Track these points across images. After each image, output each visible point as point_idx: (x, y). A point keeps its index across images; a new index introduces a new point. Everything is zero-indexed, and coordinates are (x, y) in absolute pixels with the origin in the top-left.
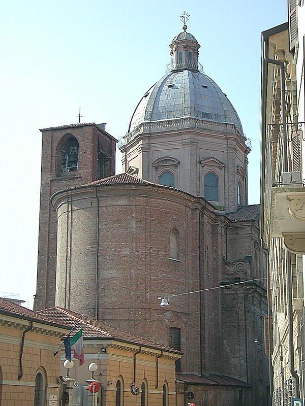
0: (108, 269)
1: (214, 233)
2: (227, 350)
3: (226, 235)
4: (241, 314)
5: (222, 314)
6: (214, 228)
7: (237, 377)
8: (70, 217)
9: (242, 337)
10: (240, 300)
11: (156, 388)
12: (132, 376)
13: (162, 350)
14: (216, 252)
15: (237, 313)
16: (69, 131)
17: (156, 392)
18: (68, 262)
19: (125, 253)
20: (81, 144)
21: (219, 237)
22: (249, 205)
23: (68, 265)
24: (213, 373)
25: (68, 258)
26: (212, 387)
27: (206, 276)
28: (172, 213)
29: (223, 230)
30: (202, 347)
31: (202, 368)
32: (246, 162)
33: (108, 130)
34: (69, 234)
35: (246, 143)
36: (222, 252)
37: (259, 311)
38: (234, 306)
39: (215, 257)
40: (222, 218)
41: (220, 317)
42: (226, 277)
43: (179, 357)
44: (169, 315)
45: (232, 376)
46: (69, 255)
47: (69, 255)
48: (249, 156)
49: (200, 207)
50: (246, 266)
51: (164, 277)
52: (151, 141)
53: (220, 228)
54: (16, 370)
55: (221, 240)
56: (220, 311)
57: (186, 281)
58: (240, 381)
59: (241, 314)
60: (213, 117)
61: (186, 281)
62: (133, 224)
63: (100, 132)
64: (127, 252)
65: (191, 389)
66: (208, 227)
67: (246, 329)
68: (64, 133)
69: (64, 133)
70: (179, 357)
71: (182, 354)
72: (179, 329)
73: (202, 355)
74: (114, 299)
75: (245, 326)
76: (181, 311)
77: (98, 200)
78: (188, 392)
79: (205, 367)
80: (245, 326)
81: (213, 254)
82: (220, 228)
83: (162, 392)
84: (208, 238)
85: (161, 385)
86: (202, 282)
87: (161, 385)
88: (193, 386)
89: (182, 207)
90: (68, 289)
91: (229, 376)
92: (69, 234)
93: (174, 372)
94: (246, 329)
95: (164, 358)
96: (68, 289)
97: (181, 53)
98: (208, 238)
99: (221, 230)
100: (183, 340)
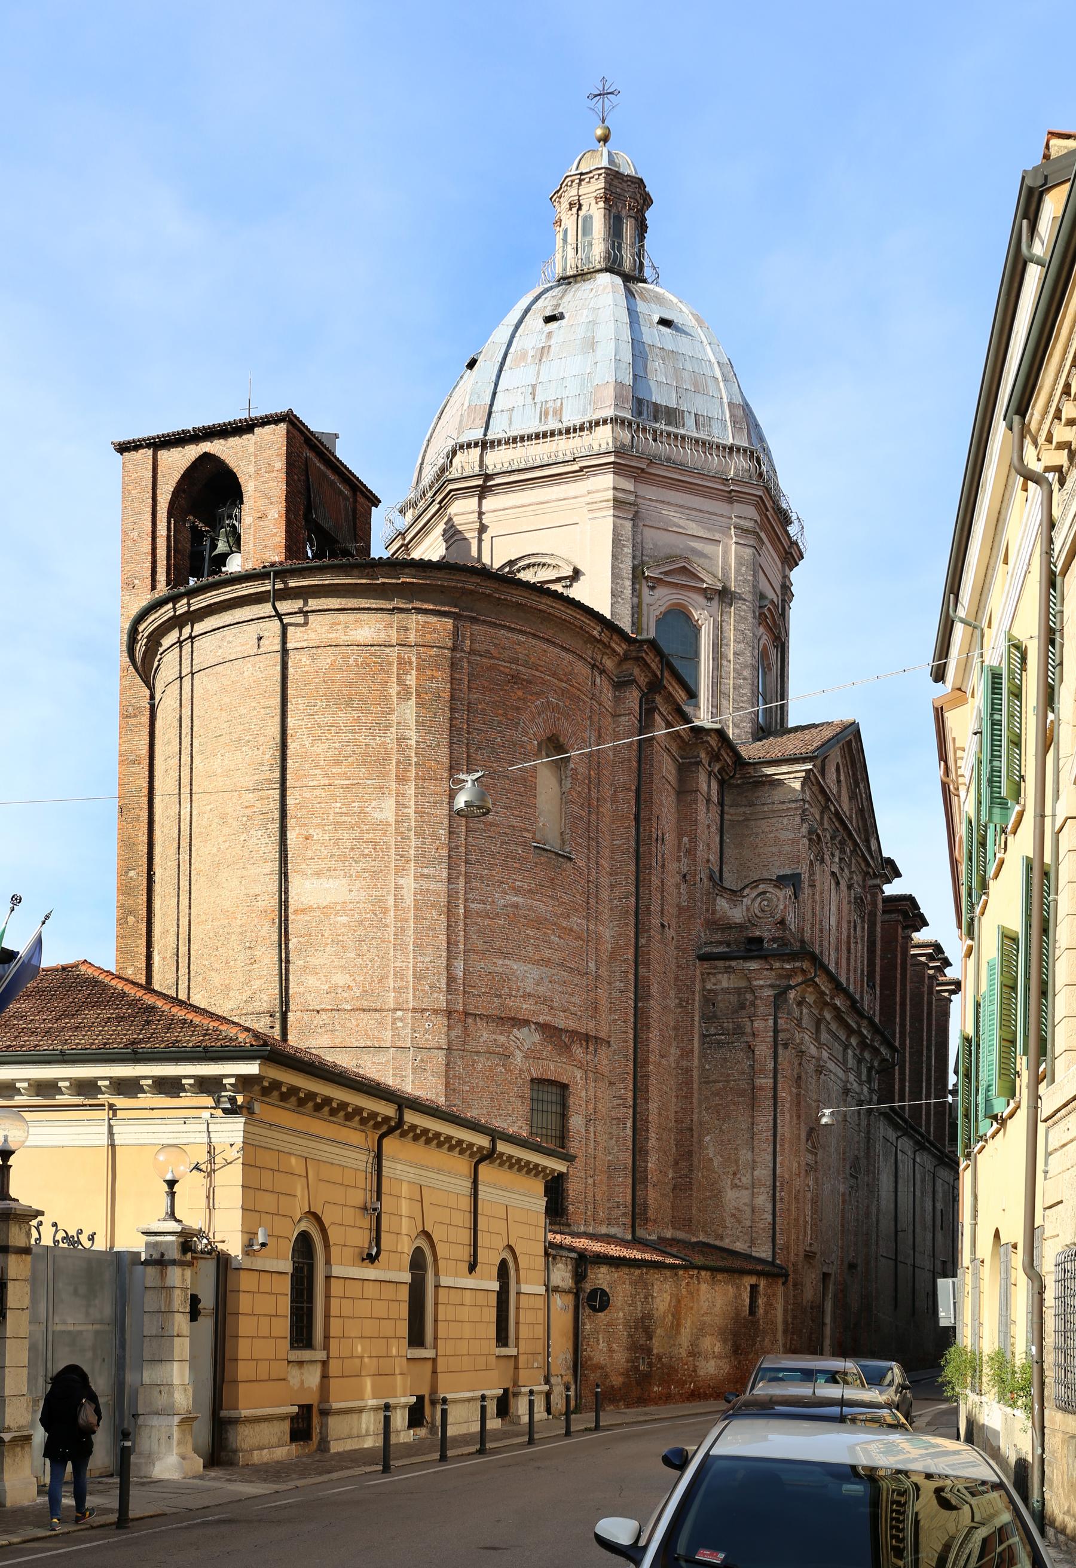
0: (318, 874)
1: (684, 791)
2: (716, 1164)
3: (721, 804)
4: (763, 1050)
5: (703, 1056)
6: (685, 770)
7: (740, 1246)
8: (186, 696)
9: (764, 1123)
10: (762, 1010)
11: (472, 1267)
12: (465, 1236)
13: (494, 1135)
14: (690, 852)
15: (751, 1049)
16: (206, 447)
17: (470, 1282)
18: (185, 857)
19: (378, 816)
20: (249, 488)
21: (701, 806)
22: (790, 725)
23: (184, 867)
24: (669, 1234)
25: (184, 844)
26: (668, 1273)
27: (656, 921)
28: (544, 683)
29: (714, 785)
30: (638, 1151)
31: (638, 1214)
32: (786, 590)
33: (343, 453)
34: (186, 759)
35: (792, 530)
36: (707, 851)
37: (813, 1050)
38: (739, 1031)
39: (684, 870)
40: (713, 741)
41: (696, 1062)
42: (718, 936)
43: (560, 1167)
44: (529, 1037)
45: (726, 1243)
46: (185, 832)
47: (185, 832)
48: (795, 575)
49: (643, 680)
50: (781, 897)
51: (516, 906)
52: (489, 503)
53: (702, 778)
54: (465, 1253)
55: (706, 817)
56: (696, 1044)
57: (592, 927)
58: (750, 1256)
59: (763, 1050)
60: (690, 422)
61: (592, 927)
62: (409, 711)
63: (311, 455)
64: (386, 811)
65: (601, 1277)
66: (666, 768)
67: (775, 1097)
68: (192, 452)
69: (192, 452)
70: (560, 1167)
71: (569, 1158)
72: (564, 1087)
73: (638, 1177)
74: (341, 979)
75: (775, 1088)
76: (572, 1025)
77: (284, 628)
78: (588, 1287)
79: (645, 1212)
80: (775, 1088)
81: (679, 861)
82: (702, 778)
83: (495, 1286)
84: (666, 805)
85: (490, 1258)
86: (643, 941)
87: (490, 1258)
88: (604, 1269)
89: (582, 669)
90: (183, 950)
91: (718, 1243)
92: (186, 759)
93: (542, 1219)
94: (775, 1097)
95: (501, 1165)
96: (183, 950)
97: (587, 220)
98: (666, 805)
99: (706, 784)
100: (576, 1122)
